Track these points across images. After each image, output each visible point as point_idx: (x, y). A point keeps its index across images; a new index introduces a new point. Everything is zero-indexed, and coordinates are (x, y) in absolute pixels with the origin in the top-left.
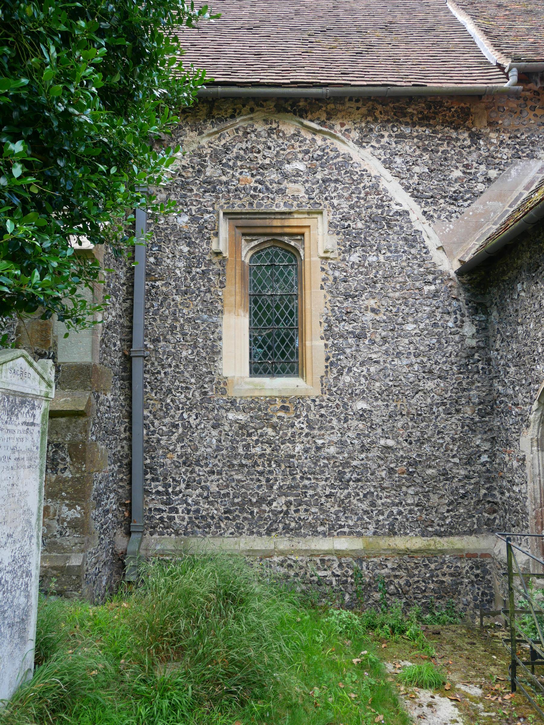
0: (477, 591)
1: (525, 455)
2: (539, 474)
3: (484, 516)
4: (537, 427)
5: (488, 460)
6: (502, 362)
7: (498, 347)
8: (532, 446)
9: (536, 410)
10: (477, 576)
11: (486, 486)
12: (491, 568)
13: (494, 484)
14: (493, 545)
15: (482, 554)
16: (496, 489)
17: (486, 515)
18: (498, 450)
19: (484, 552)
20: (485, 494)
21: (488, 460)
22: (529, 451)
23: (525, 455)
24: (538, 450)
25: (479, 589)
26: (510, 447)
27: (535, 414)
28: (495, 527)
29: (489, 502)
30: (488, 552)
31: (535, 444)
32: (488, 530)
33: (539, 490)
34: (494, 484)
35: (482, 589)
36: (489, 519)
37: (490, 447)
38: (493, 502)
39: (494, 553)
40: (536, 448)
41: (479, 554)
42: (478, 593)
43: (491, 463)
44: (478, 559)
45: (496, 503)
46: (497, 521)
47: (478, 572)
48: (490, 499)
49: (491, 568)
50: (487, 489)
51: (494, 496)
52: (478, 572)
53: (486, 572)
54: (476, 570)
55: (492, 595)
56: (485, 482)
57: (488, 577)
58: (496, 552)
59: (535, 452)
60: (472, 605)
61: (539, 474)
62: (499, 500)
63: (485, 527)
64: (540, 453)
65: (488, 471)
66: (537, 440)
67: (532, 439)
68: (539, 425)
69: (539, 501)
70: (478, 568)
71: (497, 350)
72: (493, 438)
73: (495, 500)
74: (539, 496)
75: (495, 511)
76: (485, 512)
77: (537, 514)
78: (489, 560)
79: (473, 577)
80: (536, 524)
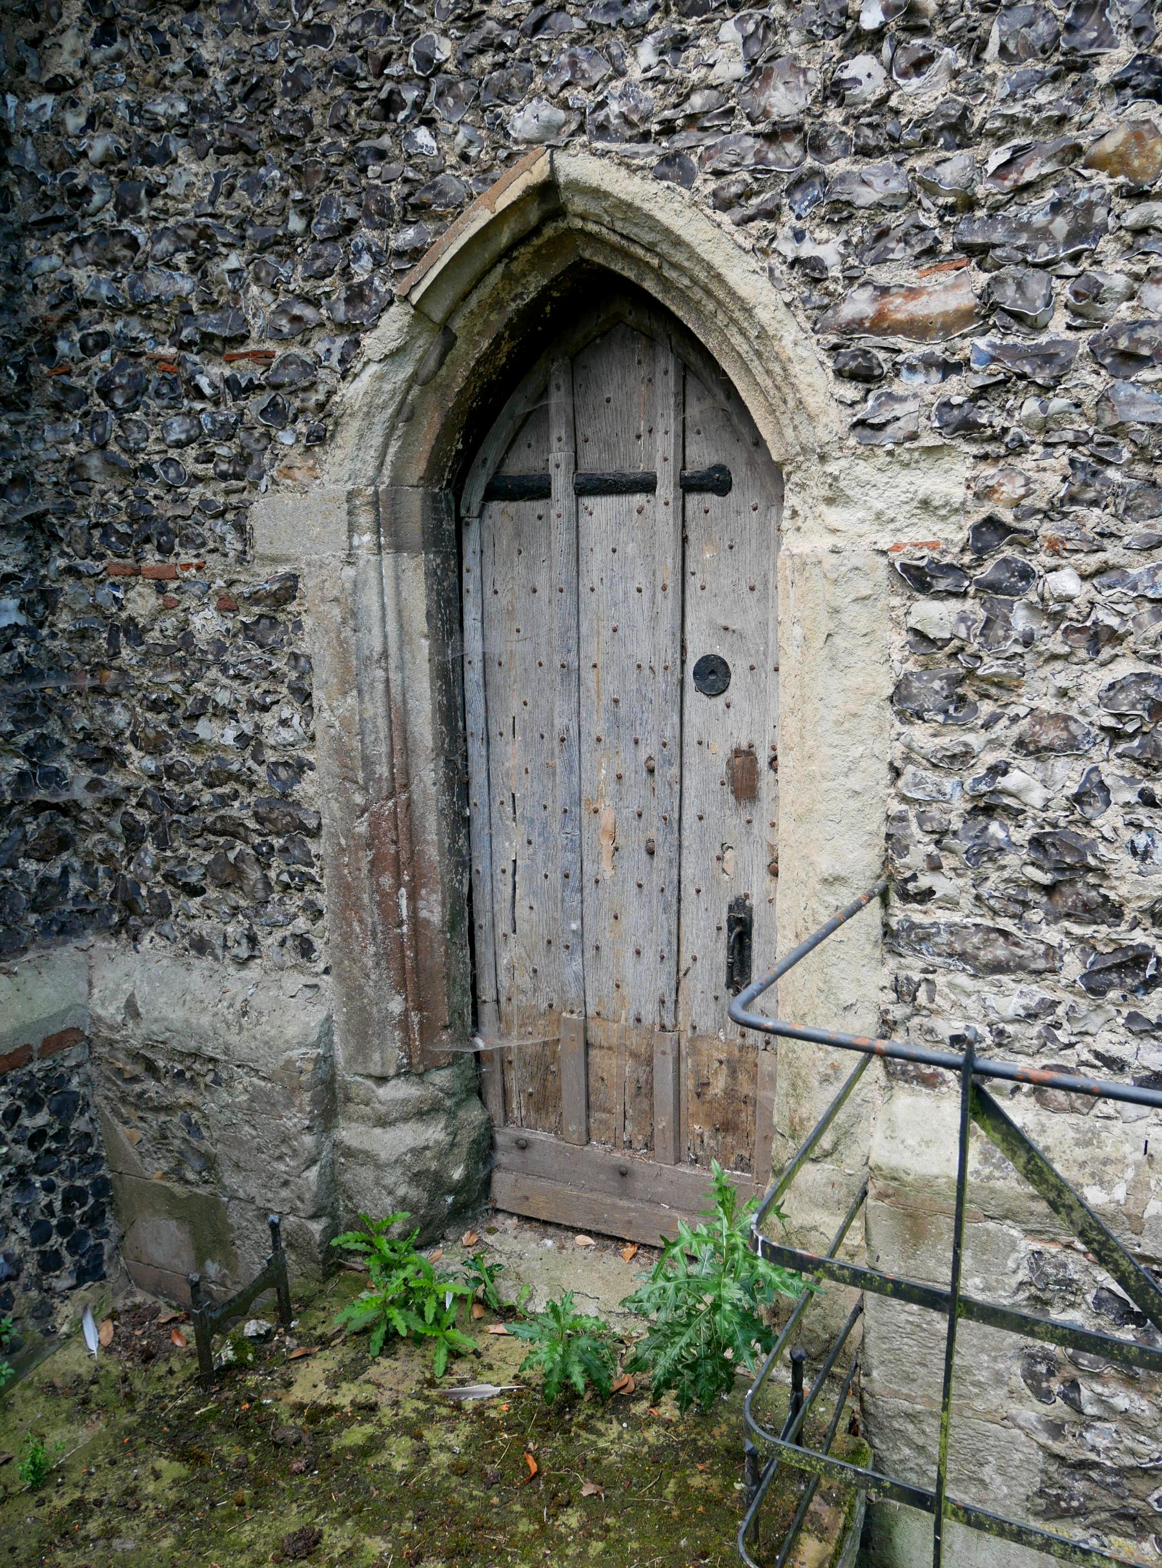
0: (43, 1199)
1: (294, 578)
2: (385, 655)
3: (24, 873)
4: (376, 440)
5: (22, 620)
6: (99, 145)
7: (64, 62)
8: (352, 529)
9: (392, 356)
10: (36, 1139)
11: (21, 740)
12: (87, 1082)
13: (54, 726)
14: (83, 987)
15: (47, 1042)
16: (60, 745)
17: (31, 866)
18: (71, 571)
19: (55, 1029)
20: (22, 776)
21: (22, 620)
22: (332, 554)
23: (294, 578)
24: (379, 547)
25: (49, 1187)
26: (165, 550)
27: (381, 377)
28: (69, 907)
29: (40, 807)
30: (69, 1023)
31: (365, 518)
32: (46, 930)
33: (382, 723)
34: (54, 726)
35: (62, 1184)
36: (45, 882)
37: (23, 559)
38: (56, 806)
39: (97, 1020)
40: (367, 538)
41: (36, 1043)
42: (49, 1206)
43: (31, 632)
44: (34, 1067)
45: (69, 810)
46: (75, 882)
47: (42, 1118)
48: (41, 794)
49: (87, 1082)
50: (29, 750)
51: (55, 778)
52: (42, 1118)
53: (67, 1106)
54: (32, 1114)
55: (102, 1187)
56: (15, 722)
57: (80, 1124)
58: (111, 1012)
59: (365, 555)
60: (30, 1267)
61: (385, 655)
62: (78, 792)
63: (32, 918)
64: (388, 559)
65: (24, 671)
66: (375, 503)
67: (351, 496)
68: (393, 428)
69: (383, 770)
70: (35, 1105)
71: (57, 86)
72: (37, 520)
73: (63, 797)
74: (383, 749)
75: (64, 843)
76: (27, 856)
77: (374, 825)
78: (74, 1054)
79: (22, 1152)
80: (375, 866)
